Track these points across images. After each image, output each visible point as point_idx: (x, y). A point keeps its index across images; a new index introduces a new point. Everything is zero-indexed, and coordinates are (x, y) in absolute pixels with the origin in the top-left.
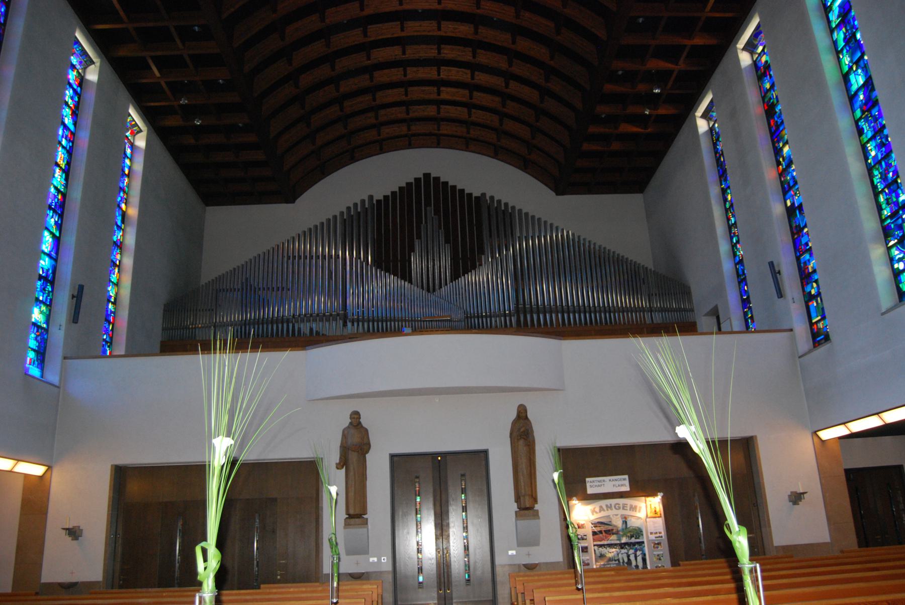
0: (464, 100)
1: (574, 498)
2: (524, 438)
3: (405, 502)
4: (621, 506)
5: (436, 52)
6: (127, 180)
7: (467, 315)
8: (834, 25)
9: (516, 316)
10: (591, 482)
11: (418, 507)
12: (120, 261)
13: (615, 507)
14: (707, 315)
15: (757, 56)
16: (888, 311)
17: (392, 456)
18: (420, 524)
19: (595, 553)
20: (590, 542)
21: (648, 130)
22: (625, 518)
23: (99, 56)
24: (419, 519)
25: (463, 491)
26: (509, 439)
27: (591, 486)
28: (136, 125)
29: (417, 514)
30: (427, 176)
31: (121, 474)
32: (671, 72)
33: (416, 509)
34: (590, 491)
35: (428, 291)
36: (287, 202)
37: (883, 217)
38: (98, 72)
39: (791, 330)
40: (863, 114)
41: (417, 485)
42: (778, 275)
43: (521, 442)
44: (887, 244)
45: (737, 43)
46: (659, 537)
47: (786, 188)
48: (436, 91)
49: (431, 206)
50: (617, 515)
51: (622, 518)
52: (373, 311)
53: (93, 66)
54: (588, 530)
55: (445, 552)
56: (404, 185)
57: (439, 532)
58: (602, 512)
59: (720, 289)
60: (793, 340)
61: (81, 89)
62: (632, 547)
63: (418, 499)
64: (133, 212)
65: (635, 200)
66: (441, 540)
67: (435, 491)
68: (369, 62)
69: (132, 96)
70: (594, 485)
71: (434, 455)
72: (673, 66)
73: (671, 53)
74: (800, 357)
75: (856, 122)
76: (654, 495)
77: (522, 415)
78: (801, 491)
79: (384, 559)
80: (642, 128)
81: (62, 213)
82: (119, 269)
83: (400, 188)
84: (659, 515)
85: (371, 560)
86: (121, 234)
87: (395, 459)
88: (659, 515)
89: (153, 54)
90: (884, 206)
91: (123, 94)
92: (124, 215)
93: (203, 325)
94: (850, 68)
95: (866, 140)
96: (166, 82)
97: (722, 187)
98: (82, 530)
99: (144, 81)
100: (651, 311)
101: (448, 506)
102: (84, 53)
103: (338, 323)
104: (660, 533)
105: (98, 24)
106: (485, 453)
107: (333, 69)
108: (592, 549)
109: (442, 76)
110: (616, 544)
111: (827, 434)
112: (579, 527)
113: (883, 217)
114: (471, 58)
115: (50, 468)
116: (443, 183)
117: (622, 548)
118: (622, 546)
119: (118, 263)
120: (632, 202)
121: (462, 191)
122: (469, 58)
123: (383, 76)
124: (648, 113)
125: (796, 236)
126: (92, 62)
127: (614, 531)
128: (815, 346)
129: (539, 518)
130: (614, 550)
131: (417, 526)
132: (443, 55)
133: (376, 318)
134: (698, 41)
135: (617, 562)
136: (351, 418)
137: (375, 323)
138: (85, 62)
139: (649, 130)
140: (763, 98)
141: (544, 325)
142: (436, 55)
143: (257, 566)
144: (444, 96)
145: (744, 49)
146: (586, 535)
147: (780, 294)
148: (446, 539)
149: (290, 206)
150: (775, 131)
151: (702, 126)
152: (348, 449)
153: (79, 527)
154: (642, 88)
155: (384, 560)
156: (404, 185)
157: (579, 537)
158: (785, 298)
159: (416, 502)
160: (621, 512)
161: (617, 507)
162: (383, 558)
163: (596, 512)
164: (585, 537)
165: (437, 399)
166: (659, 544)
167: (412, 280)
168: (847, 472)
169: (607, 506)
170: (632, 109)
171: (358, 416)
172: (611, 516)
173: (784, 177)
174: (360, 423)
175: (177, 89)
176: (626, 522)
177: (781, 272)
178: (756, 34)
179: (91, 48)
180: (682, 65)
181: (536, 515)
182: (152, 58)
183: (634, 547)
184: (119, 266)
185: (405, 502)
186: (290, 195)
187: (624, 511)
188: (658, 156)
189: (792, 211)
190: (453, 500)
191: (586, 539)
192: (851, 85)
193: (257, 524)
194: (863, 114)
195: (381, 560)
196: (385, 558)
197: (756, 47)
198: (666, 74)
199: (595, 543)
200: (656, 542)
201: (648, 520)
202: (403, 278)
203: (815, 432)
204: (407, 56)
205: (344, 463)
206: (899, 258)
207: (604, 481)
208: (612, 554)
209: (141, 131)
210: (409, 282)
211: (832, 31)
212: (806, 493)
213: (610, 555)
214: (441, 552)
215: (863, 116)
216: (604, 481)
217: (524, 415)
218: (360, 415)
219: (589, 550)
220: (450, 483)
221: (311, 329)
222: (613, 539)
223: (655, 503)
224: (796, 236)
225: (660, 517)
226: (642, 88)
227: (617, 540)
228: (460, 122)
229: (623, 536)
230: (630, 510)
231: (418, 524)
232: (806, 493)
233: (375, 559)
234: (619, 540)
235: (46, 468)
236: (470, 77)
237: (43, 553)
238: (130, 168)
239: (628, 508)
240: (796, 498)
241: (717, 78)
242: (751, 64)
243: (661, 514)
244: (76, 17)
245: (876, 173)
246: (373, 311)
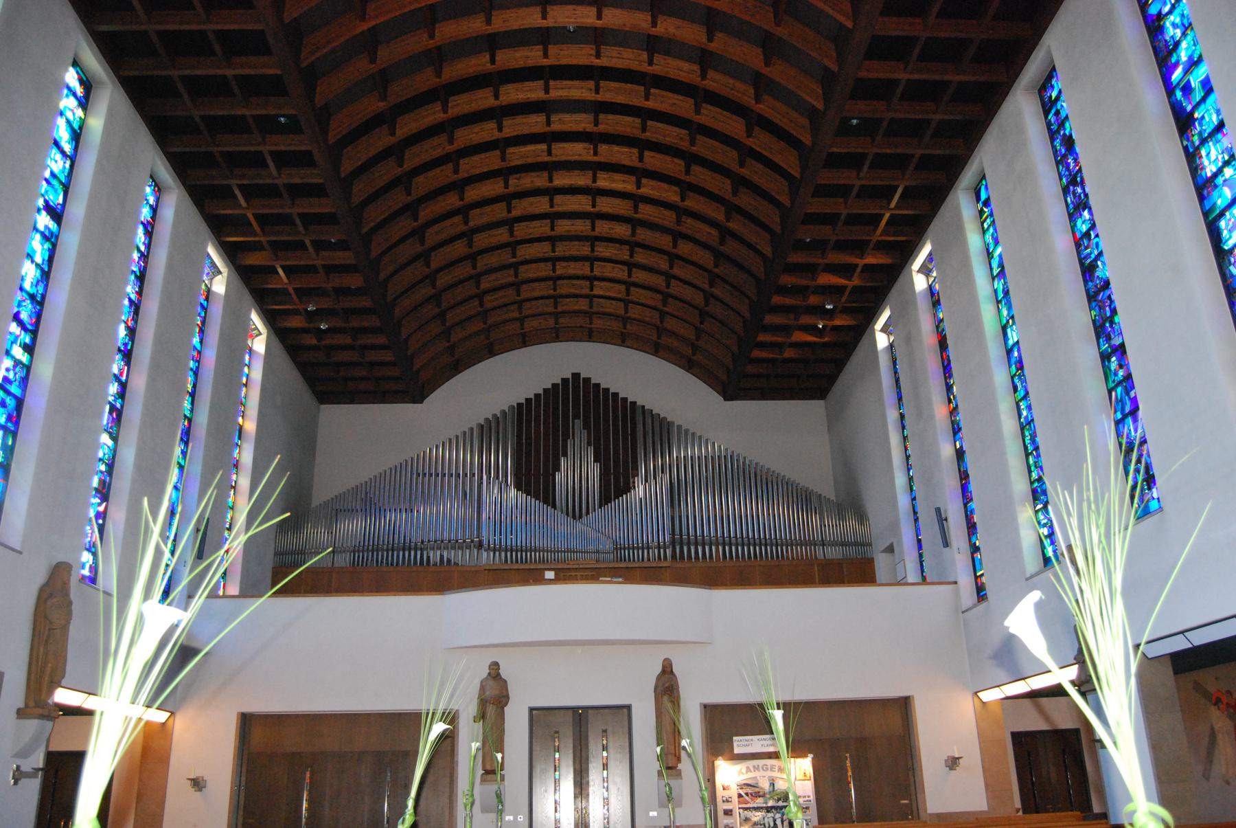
0: (620, 296)
1: (720, 758)
2: (668, 694)
3: (543, 759)
4: (769, 767)
5: (590, 249)
6: (244, 389)
7: (617, 545)
8: (995, 274)
9: (671, 549)
10: (738, 741)
11: (557, 764)
12: (235, 482)
13: (763, 768)
14: (883, 552)
15: (933, 279)
16: (1032, 577)
17: (531, 710)
18: (559, 781)
19: (740, 817)
20: (735, 805)
21: (824, 338)
22: (773, 780)
23: (228, 266)
24: (557, 777)
25: (605, 748)
26: (653, 694)
27: (738, 746)
28: (256, 328)
29: (555, 771)
30: (576, 376)
31: (247, 721)
32: (844, 288)
33: (555, 766)
34: (737, 750)
35: (574, 517)
36: (414, 402)
37: (1032, 480)
38: (225, 284)
39: (956, 583)
40: (1017, 371)
41: (557, 740)
42: (944, 522)
43: (666, 698)
44: (1035, 507)
45: (912, 264)
46: (808, 801)
47: (956, 430)
48: (588, 285)
49: (579, 418)
50: (764, 777)
51: (769, 780)
52: (512, 539)
53: (220, 276)
54: (734, 792)
55: (584, 812)
56: (550, 387)
57: (578, 790)
58: (749, 773)
59: (895, 526)
60: (957, 595)
61: (208, 302)
62: (778, 811)
63: (557, 755)
64: (250, 426)
65: (815, 408)
66: (580, 799)
67: (574, 747)
68: (515, 260)
69: (158, 143)
70: (742, 744)
71: (574, 709)
72: (846, 282)
73: (846, 270)
74: (963, 612)
75: (1012, 378)
76: (805, 756)
77: (667, 670)
78: (957, 756)
79: (521, 818)
80: (816, 337)
81: (188, 439)
82: (235, 491)
83: (545, 390)
84: (808, 778)
85: (507, 818)
86: (237, 451)
87: (534, 712)
88: (808, 778)
89: (239, 182)
90: (1033, 468)
91: (248, 298)
92: (241, 428)
93: (317, 550)
94: (1008, 322)
95: (1019, 398)
96: (294, 289)
97: (901, 411)
98: (206, 781)
99: (271, 286)
100: (823, 545)
101: (588, 764)
102: (213, 264)
103: (472, 551)
104: (809, 797)
105: (228, 237)
106: (628, 708)
107: (456, 171)
108: (736, 811)
109: (595, 273)
110: (762, 808)
111: (989, 696)
112: (724, 789)
113: (1032, 480)
114: (628, 257)
115: (172, 713)
116: (594, 384)
117: (768, 812)
118: (769, 809)
119: (233, 484)
120: (810, 411)
121: (616, 395)
122: (625, 257)
123: (515, 126)
124: (821, 327)
125: (964, 482)
126: (220, 272)
127: (761, 793)
128: (979, 602)
129: (681, 778)
130: (760, 813)
131: (555, 784)
132: (598, 253)
133: (514, 548)
134: (870, 260)
135: (763, 826)
136: (489, 669)
137: (514, 554)
138: (213, 273)
139: (826, 339)
140: (937, 327)
141: (703, 558)
142: (589, 253)
143: (388, 822)
144: (597, 272)
145: (919, 271)
146: (731, 798)
147: (946, 544)
148: (585, 798)
149: (418, 406)
150: (947, 366)
151: (882, 341)
152: (486, 702)
153: (203, 777)
154: (814, 300)
155: (520, 818)
156: (550, 387)
157: (724, 799)
158: (951, 547)
159: (555, 758)
160: (769, 773)
161: (765, 768)
162: (519, 817)
163: (743, 773)
164: (730, 799)
165: (579, 650)
166: (807, 808)
167: (556, 505)
168: (1016, 736)
169: (754, 767)
170: (806, 320)
171: (497, 667)
172: (758, 778)
173: (955, 416)
174: (499, 674)
175: (303, 293)
176: (774, 784)
177: (948, 520)
178: (930, 258)
179: (221, 255)
180: (856, 281)
181: (679, 775)
182: (241, 187)
183: (781, 811)
184: (234, 488)
185: (543, 759)
186: (417, 393)
187: (772, 772)
188: (840, 365)
189: (960, 454)
190: (594, 757)
191: (731, 801)
192: (1008, 339)
193: (389, 779)
194: (1017, 371)
195: (517, 819)
196: (522, 817)
197: (930, 271)
198: (840, 290)
199: (741, 806)
200: (804, 806)
201: (797, 782)
202: (546, 501)
203: (976, 693)
204: (556, 254)
205: (482, 716)
206: (1044, 524)
207: (752, 740)
208: (758, 818)
209: (260, 334)
210: (552, 507)
211: (993, 279)
212: (961, 758)
213: (755, 819)
214: (580, 812)
215: (1017, 374)
216: (752, 740)
217: (669, 669)
218: (499, 666)
219: (734, 812)
220: (590, 739)
221: (442, 556)
222: (759, 802)
223: (804, 765)
224: (964, 482)
225: (810, 780)
226: (814, 300)
227: (764, 803)
228: (621, 242)
229: (769, 799)
230: (778, 771)
231: (557, 783)
232: (961, 758)
233: (511, 818)
234: (766, 803)
235: (169, 714)
236: (627, 274)
237: (164, 803)
238: (248, 376)
239: (776, 770)
240: (953, 763)
241: (937, 225)
242: (927, 288)
243: (810, 777)
244: (125, 95)
245: (1027, 433)
246: (512, 539)
